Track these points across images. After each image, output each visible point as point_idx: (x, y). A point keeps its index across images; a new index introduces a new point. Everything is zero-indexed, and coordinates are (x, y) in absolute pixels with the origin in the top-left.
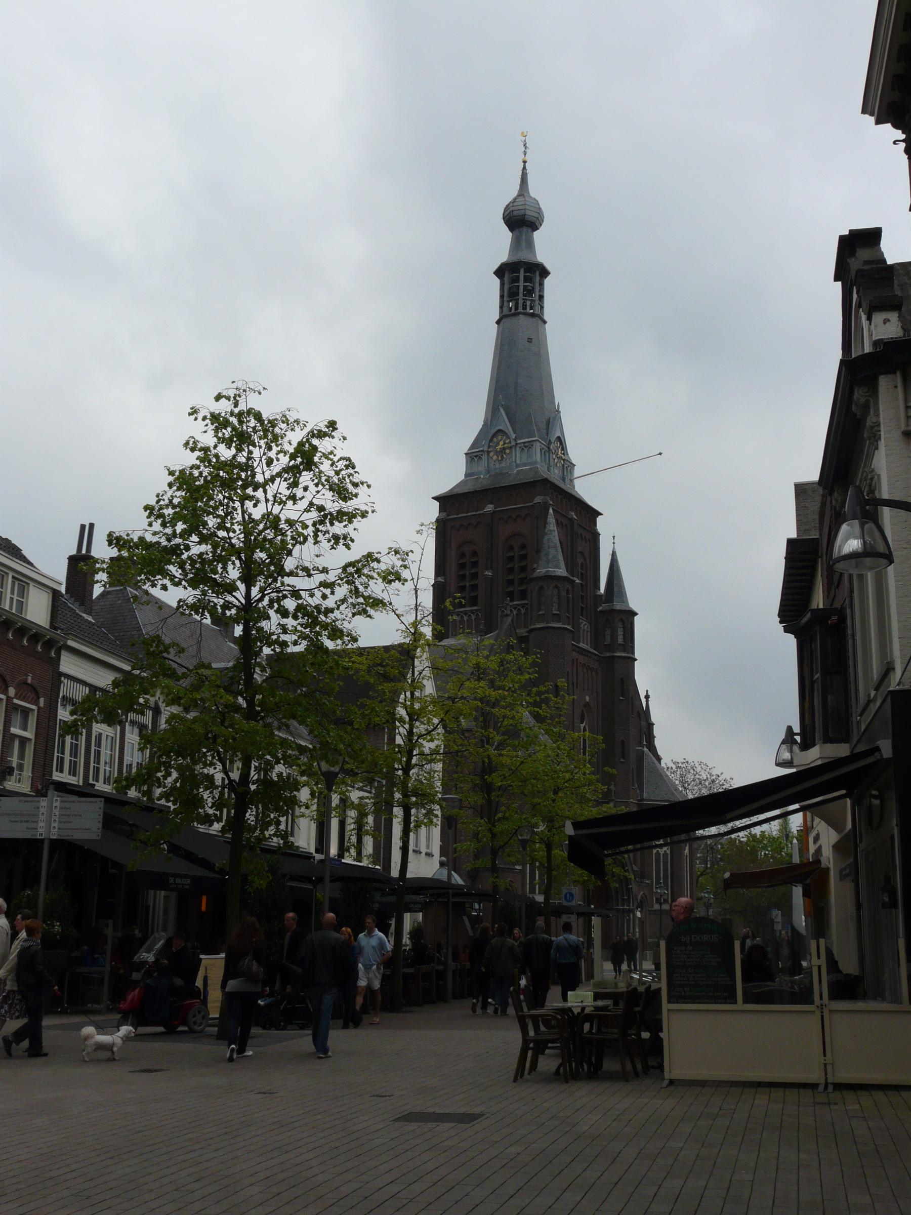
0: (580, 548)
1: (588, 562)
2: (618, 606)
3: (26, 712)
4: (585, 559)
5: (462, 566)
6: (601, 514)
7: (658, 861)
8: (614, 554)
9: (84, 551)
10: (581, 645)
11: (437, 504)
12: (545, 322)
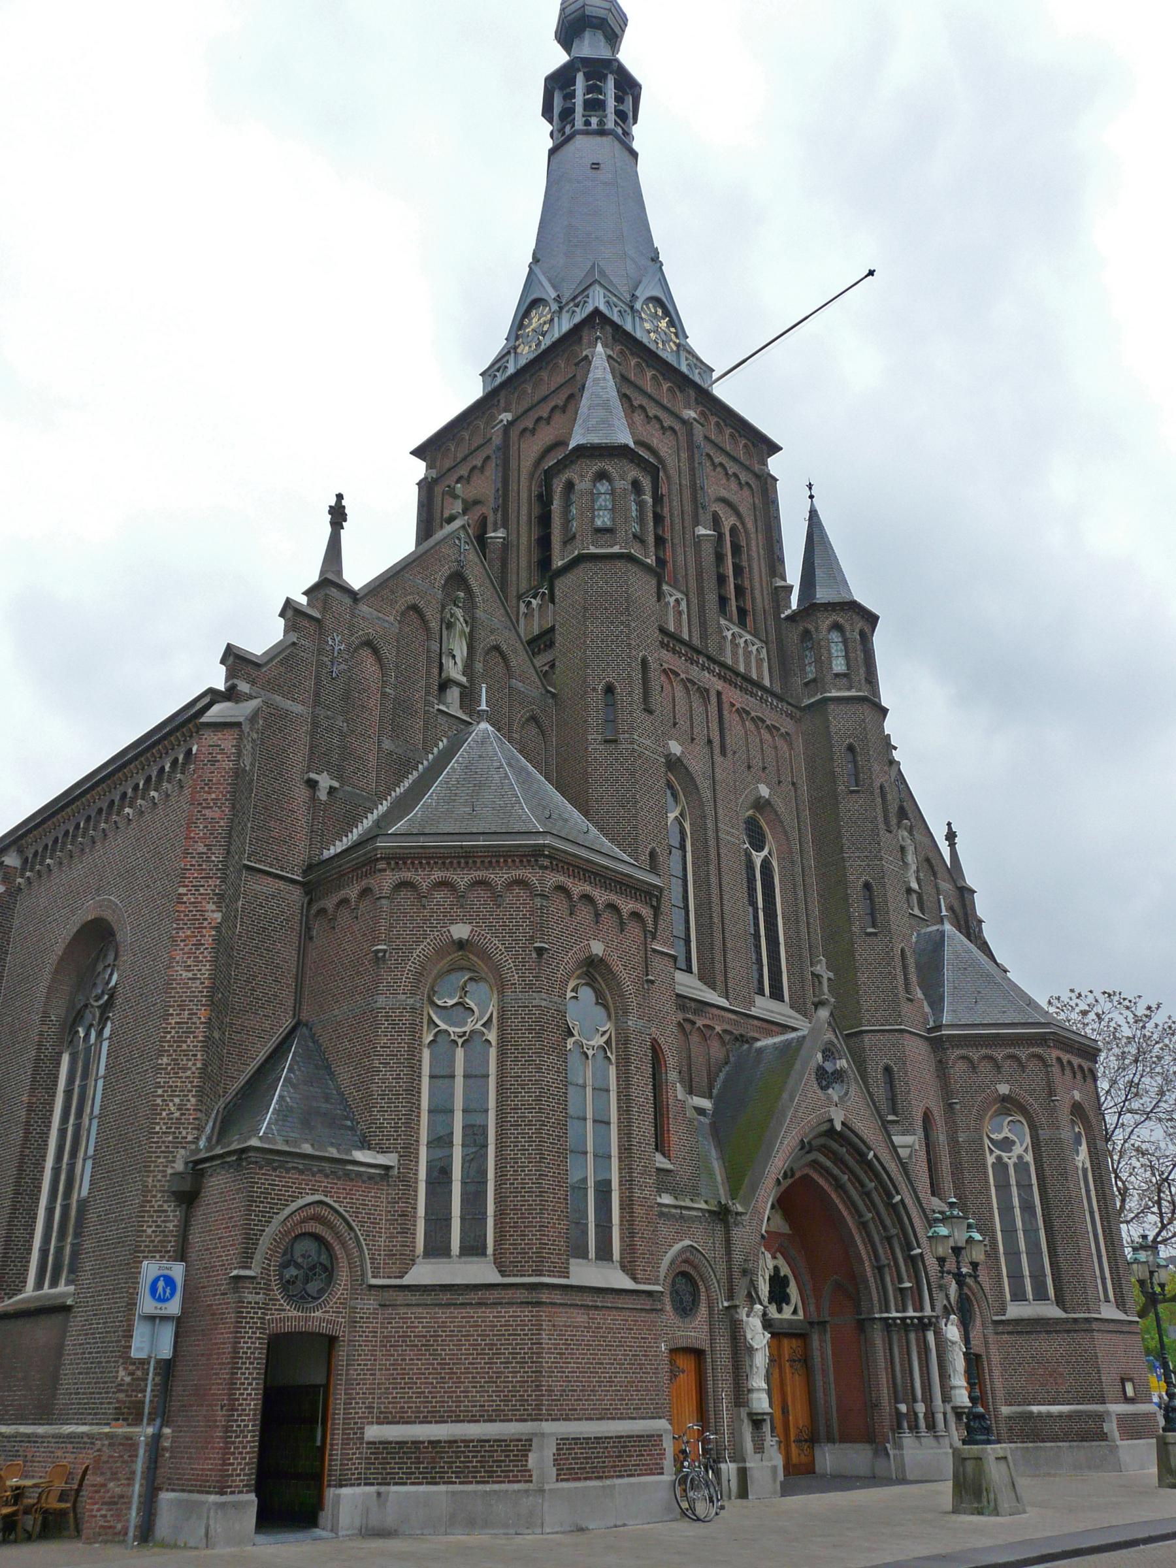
1: (750, 525)
4: (738, 515)
6: (781, 449)
7: (1003, 1187)
12: (884, 711)
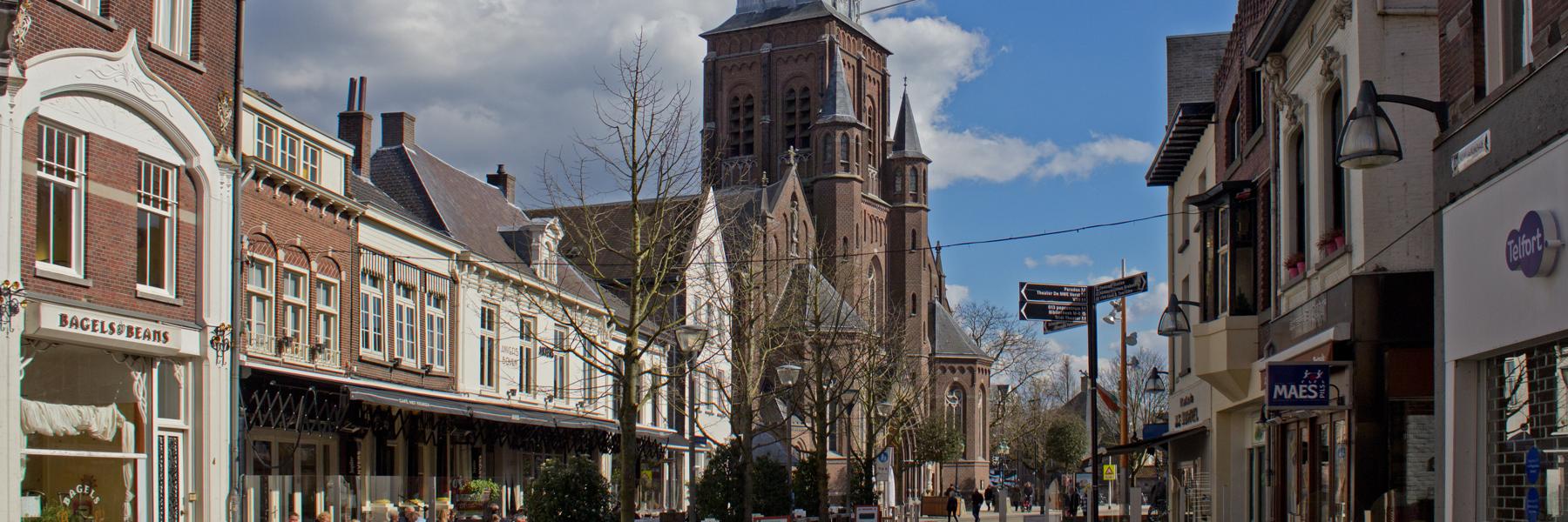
0: (868, 92)
2: (909, 151)
3: (296, 276)
5: (735, 110)
8: (905, 97)
9: (356, 108)
10: (870, 195)
11: (704, 42)
12: (1343, 27)
